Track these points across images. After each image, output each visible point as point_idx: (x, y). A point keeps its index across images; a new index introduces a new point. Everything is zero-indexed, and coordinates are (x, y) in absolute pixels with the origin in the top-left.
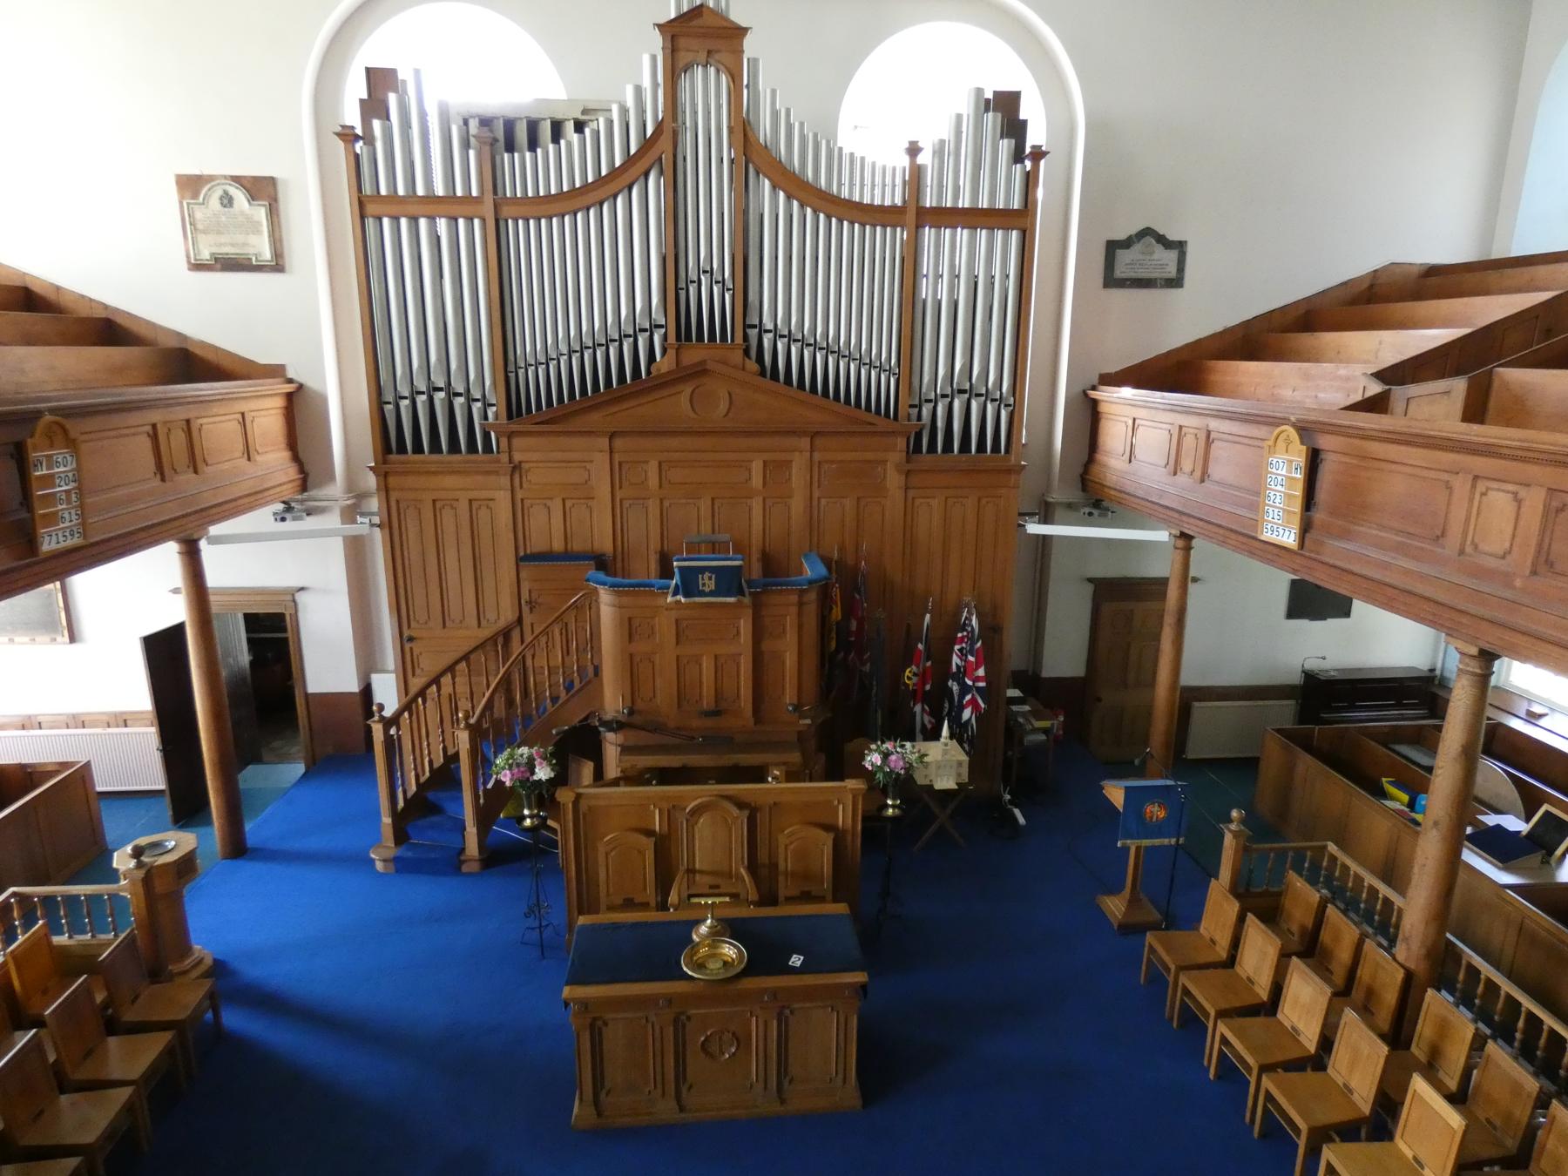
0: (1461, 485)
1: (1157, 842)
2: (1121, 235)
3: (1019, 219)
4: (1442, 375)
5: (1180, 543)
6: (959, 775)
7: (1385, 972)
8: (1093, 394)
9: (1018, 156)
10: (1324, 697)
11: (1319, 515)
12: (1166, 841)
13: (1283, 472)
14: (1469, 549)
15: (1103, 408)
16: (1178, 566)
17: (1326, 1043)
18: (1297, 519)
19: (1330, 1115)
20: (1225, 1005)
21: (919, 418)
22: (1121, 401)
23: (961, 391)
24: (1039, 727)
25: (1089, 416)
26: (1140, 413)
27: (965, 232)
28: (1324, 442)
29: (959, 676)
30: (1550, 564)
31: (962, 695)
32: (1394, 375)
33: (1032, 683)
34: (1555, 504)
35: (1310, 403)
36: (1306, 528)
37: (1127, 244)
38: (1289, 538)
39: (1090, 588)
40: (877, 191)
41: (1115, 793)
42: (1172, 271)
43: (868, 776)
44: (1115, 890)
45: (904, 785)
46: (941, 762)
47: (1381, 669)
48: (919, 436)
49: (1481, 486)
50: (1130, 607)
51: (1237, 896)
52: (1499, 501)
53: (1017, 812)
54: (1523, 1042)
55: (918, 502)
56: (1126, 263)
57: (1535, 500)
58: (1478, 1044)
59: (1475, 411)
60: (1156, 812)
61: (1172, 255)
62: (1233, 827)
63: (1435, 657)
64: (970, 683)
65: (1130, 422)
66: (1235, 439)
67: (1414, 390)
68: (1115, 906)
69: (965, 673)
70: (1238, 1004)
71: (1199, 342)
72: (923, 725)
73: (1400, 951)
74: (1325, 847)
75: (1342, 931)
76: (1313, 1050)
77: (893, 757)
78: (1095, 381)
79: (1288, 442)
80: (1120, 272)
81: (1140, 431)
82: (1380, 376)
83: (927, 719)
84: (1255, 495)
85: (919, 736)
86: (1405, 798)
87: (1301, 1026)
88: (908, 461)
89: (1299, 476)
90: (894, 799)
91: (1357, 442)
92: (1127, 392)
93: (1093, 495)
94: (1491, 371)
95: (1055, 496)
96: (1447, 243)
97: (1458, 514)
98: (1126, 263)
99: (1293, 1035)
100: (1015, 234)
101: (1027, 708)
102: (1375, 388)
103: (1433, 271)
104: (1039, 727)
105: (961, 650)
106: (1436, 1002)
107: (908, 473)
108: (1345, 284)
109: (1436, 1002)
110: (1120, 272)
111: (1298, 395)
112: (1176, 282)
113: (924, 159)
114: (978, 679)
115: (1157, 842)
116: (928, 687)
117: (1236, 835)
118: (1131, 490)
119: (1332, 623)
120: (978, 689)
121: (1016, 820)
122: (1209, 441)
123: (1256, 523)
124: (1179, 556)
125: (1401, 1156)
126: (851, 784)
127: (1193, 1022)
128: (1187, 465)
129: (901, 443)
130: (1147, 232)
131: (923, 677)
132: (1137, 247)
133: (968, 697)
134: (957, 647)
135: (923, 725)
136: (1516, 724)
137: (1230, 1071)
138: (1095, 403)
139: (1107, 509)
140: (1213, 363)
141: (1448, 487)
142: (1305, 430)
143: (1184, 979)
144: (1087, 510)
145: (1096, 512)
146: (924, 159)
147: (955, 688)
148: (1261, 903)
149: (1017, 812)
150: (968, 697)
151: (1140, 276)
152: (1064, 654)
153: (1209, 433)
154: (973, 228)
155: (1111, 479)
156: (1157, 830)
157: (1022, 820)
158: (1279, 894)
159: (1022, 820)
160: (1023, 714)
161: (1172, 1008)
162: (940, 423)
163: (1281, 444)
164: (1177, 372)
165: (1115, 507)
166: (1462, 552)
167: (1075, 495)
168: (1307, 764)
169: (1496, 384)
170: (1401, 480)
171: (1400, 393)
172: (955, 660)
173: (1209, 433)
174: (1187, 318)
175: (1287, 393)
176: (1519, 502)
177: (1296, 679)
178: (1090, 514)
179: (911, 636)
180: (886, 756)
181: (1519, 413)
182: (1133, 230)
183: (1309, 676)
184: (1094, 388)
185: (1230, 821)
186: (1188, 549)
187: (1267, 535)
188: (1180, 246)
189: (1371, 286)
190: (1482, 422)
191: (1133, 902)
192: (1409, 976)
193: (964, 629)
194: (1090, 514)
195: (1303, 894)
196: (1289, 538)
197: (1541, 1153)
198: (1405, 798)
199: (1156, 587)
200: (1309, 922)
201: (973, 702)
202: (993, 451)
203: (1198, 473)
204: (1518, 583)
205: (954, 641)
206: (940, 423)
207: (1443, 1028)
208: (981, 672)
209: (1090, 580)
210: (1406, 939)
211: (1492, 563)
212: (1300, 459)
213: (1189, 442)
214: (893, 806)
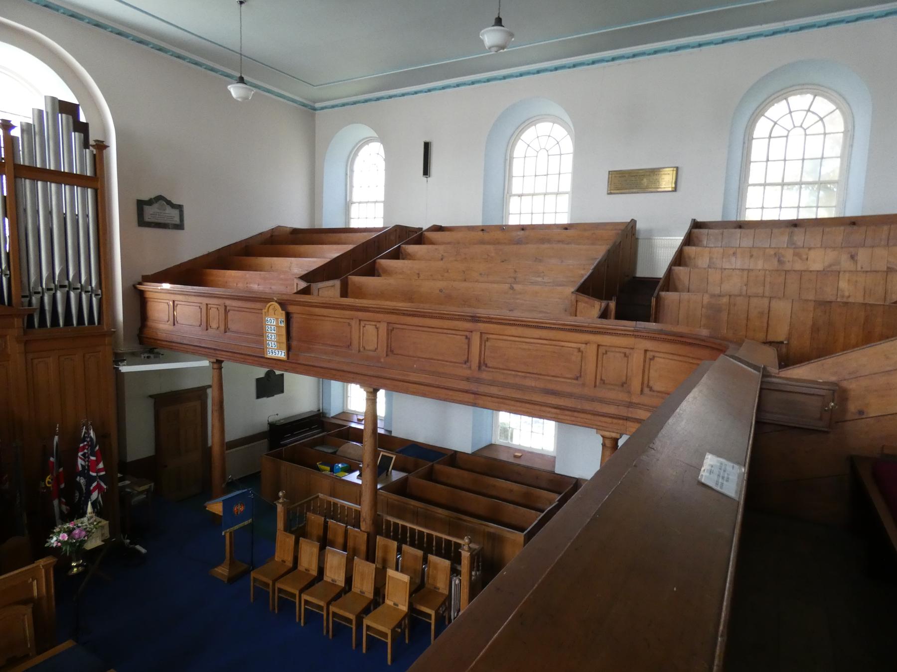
0: (354, 323)
1: (241, 525)
2: (145, 197)
3: (95, 181)
4: (329, 279)
5: (216, 366)
6: (103, 535)
7: (359, 536)
8: (141, 287)
9: (86, 144)
10: (279, 433)
11: (294, 343)
12: (246, 523)
13: (274, 325)
14: (362, 349)
15: (148, 295)
16: (216, 379)
17: (349, 580)
18: (284, 346)
19: (359, 608)
20: (302, 586)
21: (30, 304)
22: (163, 292)
23: (62, 286)
24: (140, 491)
25: (139, 302)
26: (177, 297)
27: (67, 187)
28: (292, 309)
29: (84, 473)
30: (392, 351)
31: (89, 484)
32: (311, 277)
33: (126, 468)
34: (390, 328)
35: (267, 290)
36: (289, 349)
37: (150, 202)
38: (281, 355)
39: (151, 402)
40: (26, 159)
41: (216, 507)
42: (177, 220)
43: (55, 551)
44: (219, 563)
45: (78, 549)
46: (89, 529)
47: (296, 416)
48: (31, 317)
49: (362, 323)
50: (180, 408)
51: (291, 532)
52: (370, 329)
53: (138, 547)
54: (410, 541)
55: (36, 361)
56: (150, 213)
57: (383, 327)
58: (399, 550)
59: (344, 293)
60: (239, 508)
61: (175, 213)
62: (281, 501)
63: (319, 404)
64: (94, 474)
65: (171, 303)
66: (240, 310)
67: (320, 285)
68: (222, 571)
69: (89, 470)
70: (306, 583)
71: (196, 259)
72: (61, 512)
73: (363, 526)
74: (318, 497)
75: (337, 527)
76: (343, 585)
77: (77, 531)
78: (140, 279)
79: (275, 310)
80: (147, 218)
81: (179, 308)
82: (303, 278)
83: (64, 508)
84: (260, 335)
85: (58, 520)
86: (328, 468)
87: (336, 578)
88: (25, 333)
89: (283, 325)
90: (77, 560)
91: (307, 308)
92: (166, 286)
93: (148, 344)
94: (347, 277)
95: (122, 349)
96: (296, 218)
97: (355, 336)
98: (150, 213)
99: (333, 584)
100: (90, 191)
101: (127, 482)
102: (303, 285)
103: (295, 231)
104: (140, 491)
105: (84, 455)
106: (380, 540)
107: (26, 343)
108: (261, 234)
109: (380, 540)
110: (147, 218)
111: (261, 288)
112: (180, 226)
113: (16, 132)
114: (100, 470)
115: (241, 525)
116: (63, 486)
117: (283, 504)
118: (175, 340)
119: (277, 397)
120: (101, 477)
121: (139, 552)
122: (226, 312)
123: (263, 350)
124: (216, 372)
125: (389, 606)
126: (41, 562)
127: (287, 604)
128: (214, 325)
129: (17, 322)
130: (159, 198)
131: (57, 480)
132: (156, 205)
133: (94, 484)
134: (80, 454)
135: (61, 512)
136: (353, 425)
137: (313, 616)
138: (142, 293)
139: (158, 353)
140: (208, 271)
141: (349, 324)
142: (283, 304)
143: (278, 585)
144: (146, 355)
145: (152, 356)
146: (16, 132)
147: (82, 481)
148: (299, 531)
149: (138, 547)
150: (94, 484)
151: (159, 221)
152: (139, 442)
153: (226, 307)
154: (72, 185)
155: (162, 336)
156: (242, 517)
157: (143, 551)
158: (305, 526)
159: (143, 551)
160: (128, 486)
161: (273, 605)
162: (60, 309)
163: (271, 311)
164: (189, 274)
165: (162, 351)
166: (359, 351)
167: (136, 347)
168: (286, 466)
169: (350, 282)
170: (329, 324)
171: (315, 286)
172: (80, 462)
173: (226, 307)
174: (190, 246)
175: (255, 287)
176: (377, 328)
177: (266, 428)
178: (148, 357)
179: (46, 451)
180: (70, 532)
181: (360, 293)
182: (153, 195)
183: (272, 425)
184: (140, 284)
185: (279, 498)
186: (220, 368)
187: (270, 355)
188: (180, 208)
189: (272, 236)
190: (346, 297)
191: (232, 563)
192: (368, 534)
193: (84, 440)
194: (148, 357)
195: (315, 520)
196: (281, 355)
197: (428, 577)
198: (328, 468)
199: (200, 393)
200: (321, 533)
201: (98, 487)
202: (89, 323)
203: (222, 328)
204: (382, 360)
205: (78, 450)
206: (47, 307)
207: (386, 549)
208: (101, 466)
209: (151, 396)
210: (364, 520)
211: (371, 353)
212: (282, 318)
213: (213, 312)
214: (76, 566)
